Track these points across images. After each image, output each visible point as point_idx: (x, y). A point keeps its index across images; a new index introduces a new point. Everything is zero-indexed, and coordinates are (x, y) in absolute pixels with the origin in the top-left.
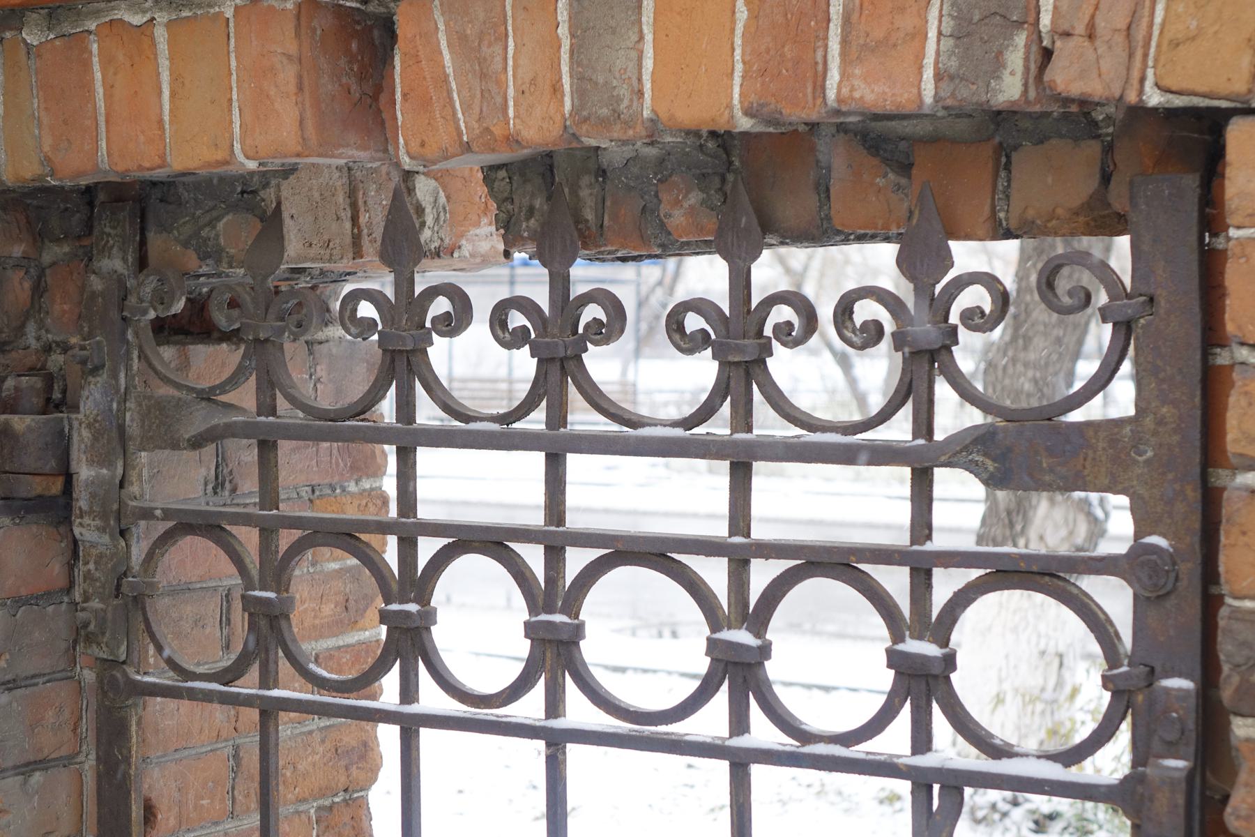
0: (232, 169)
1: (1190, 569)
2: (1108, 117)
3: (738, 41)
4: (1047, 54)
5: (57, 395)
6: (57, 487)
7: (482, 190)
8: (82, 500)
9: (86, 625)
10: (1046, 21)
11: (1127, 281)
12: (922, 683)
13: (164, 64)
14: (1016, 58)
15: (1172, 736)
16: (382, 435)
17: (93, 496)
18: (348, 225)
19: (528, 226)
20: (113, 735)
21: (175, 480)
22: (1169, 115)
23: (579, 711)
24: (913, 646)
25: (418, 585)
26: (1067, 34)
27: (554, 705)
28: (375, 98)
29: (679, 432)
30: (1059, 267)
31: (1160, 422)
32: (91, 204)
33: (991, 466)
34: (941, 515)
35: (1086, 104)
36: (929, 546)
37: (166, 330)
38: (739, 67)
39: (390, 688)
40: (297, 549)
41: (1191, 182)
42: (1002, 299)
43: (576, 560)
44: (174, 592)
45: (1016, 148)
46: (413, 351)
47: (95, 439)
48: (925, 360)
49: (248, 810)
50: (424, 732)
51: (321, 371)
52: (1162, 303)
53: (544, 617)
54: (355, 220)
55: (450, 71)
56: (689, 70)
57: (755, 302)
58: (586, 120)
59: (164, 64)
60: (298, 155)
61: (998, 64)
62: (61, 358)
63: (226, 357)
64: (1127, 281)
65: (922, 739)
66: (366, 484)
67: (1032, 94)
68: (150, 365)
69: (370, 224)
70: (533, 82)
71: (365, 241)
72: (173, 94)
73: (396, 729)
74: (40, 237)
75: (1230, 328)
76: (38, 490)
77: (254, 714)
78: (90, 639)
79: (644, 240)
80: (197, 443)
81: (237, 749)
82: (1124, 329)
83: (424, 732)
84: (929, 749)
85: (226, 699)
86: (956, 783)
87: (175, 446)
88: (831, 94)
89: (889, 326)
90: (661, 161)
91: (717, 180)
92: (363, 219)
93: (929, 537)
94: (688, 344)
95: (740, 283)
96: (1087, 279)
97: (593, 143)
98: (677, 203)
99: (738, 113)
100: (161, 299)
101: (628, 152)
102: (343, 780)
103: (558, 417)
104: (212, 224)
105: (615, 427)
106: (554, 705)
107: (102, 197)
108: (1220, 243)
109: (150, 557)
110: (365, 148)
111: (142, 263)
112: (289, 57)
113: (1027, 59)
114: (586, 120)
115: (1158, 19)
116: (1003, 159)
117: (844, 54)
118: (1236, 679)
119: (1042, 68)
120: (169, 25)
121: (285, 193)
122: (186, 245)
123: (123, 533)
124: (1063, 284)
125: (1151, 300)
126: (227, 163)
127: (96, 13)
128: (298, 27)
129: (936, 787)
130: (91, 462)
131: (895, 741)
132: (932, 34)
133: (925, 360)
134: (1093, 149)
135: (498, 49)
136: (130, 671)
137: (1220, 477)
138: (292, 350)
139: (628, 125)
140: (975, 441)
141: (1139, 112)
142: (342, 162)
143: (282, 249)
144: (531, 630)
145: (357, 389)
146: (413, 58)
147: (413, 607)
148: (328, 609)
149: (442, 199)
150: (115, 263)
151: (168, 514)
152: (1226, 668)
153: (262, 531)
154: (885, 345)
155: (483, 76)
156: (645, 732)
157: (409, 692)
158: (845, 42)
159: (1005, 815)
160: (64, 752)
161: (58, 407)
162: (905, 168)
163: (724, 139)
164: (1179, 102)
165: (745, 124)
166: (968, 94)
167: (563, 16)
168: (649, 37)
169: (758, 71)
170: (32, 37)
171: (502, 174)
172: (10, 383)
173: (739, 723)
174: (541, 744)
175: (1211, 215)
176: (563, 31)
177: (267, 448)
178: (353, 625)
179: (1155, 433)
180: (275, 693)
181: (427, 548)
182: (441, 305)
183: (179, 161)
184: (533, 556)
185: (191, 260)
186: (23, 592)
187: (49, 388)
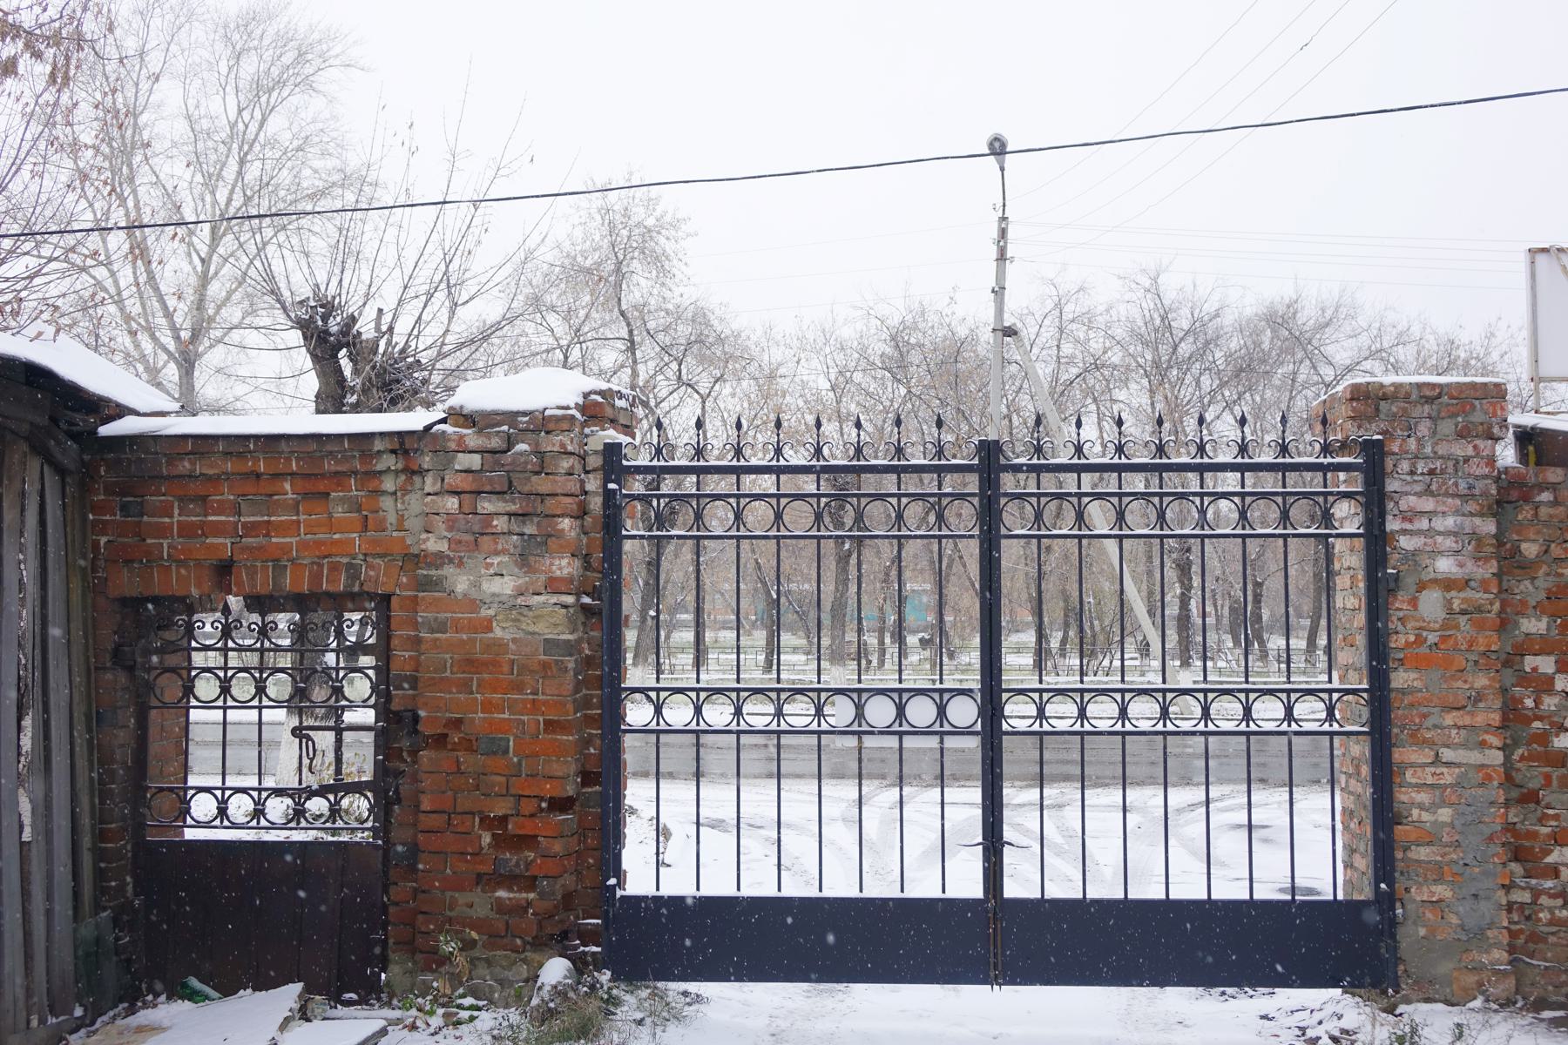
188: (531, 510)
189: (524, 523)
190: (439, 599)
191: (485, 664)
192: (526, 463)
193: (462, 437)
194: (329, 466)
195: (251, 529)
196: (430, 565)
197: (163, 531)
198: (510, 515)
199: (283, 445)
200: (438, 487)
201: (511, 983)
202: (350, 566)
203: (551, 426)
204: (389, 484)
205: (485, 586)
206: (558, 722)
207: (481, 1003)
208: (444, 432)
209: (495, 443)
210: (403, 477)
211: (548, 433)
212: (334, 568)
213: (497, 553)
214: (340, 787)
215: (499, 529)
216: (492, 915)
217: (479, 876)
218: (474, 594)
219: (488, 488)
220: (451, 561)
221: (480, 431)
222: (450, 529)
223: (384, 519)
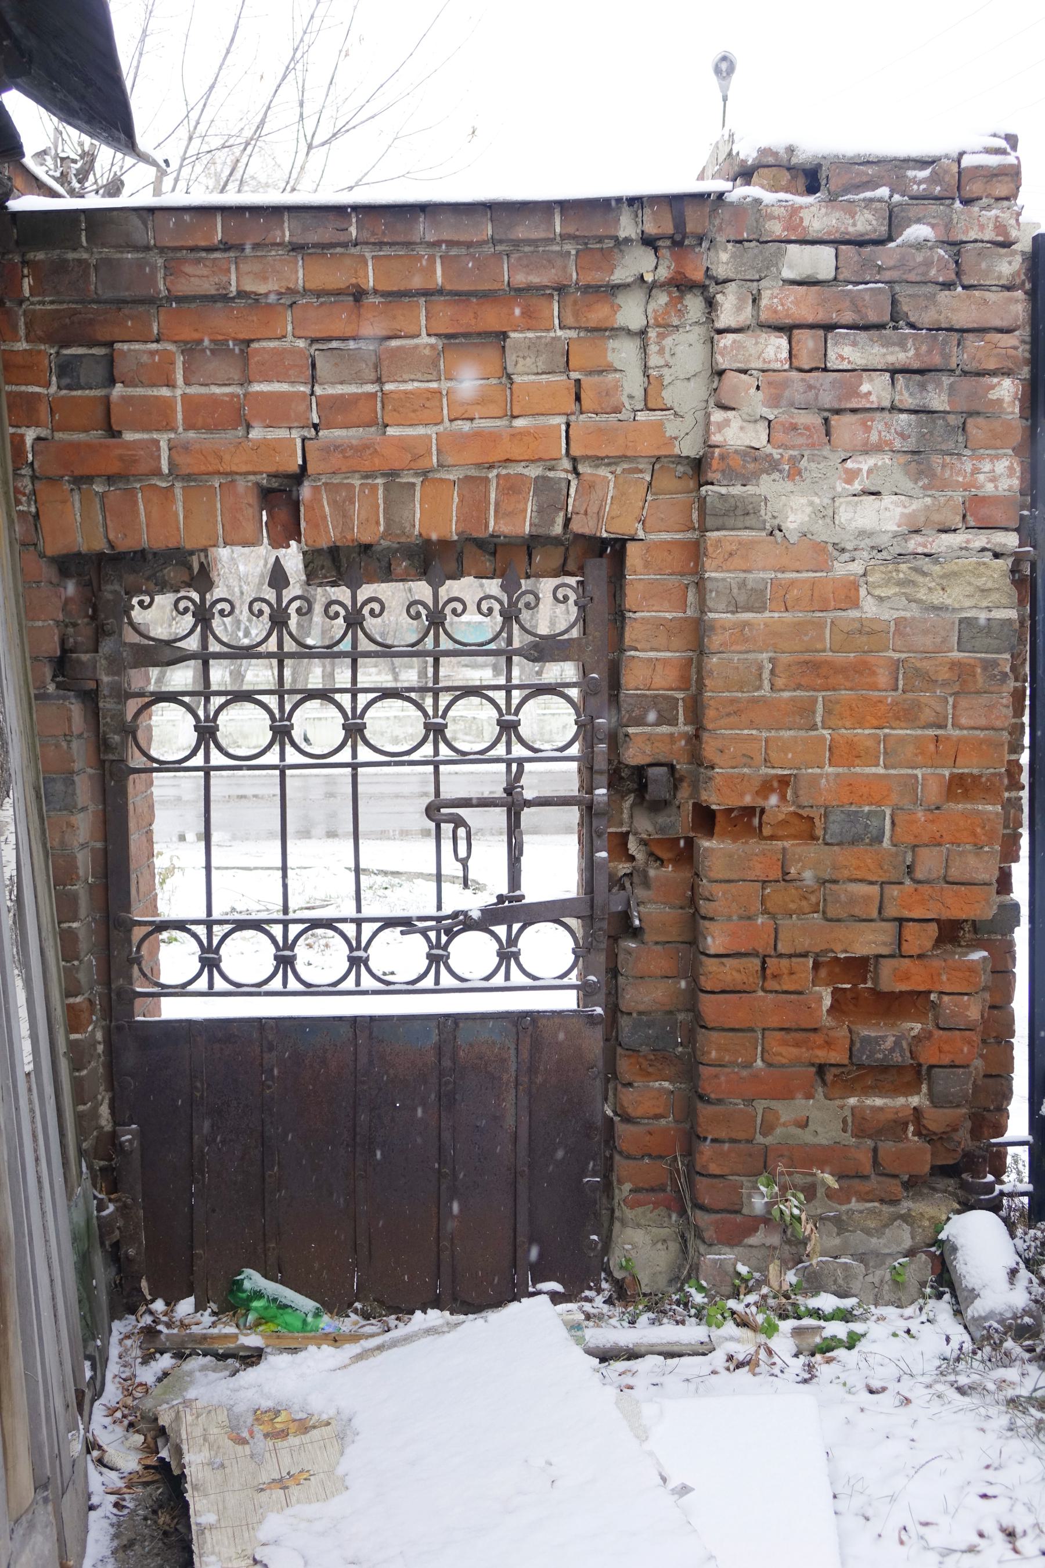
10: (570, 508)
14: (560, 520)
34: (348, 673)
52: (595, 600)
61: (553, 522)
72: (185, 517)
86: (521, 762)
106: (207, 758)
120: (183, 488)
130: (107, 675)
154: (190, 613)
155: (344, 516)
158: (496, 511)
166: (541, 531)
176: (381, 501)
188: (937, 360)
189: (923, 387)
190: (747, 546)
191: (843, 670)
192: (928, 264)
193: (795, 210)
194: (513, 273)
195: (336, 410)
196: (733, 475)
197: (158, 416)
198: (894, 372)
199: (423, 229)
200: (746, 315)
201: (880, 1258)
202: (542, 482)
203: (973, 189)
204: (631, 312)
205: (844, 515)
206: (976, 778)
207: (849, 1303)
208: (758, 201)
209: (865, 223)
210: (662, 299)
211: (966, 202)
212: (511, 487)
213: (867, 450)
214: (511, 913)
215: (874, 401)
216: (849, 1140)
217: (821, 1069)
218: (823, 533)
219: (848, 317)
220: (773, 466)
221: (832, 199)
222: (774, 402)
223: (618, 386)
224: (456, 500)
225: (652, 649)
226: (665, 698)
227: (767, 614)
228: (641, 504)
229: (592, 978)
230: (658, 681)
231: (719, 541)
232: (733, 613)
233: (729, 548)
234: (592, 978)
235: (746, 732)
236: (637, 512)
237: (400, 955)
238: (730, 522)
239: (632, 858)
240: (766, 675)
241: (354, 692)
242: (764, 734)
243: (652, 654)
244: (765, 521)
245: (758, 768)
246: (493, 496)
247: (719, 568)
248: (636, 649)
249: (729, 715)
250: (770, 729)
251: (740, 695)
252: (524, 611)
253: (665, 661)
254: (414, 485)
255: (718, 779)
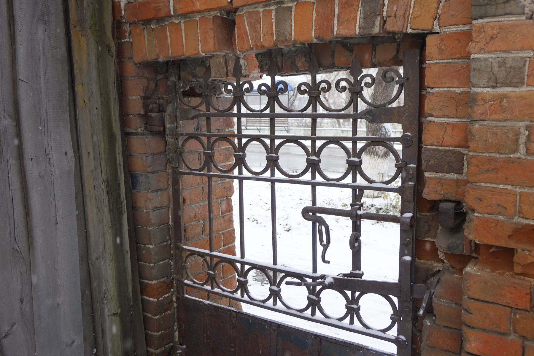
0: (199, 56)
1: (416, 140)
2: (399, 37)
3: (314, 21)
4: (385, 22)
5: (161, 109)
6: (162, 129)
7: (255, 59)
8: (167, 132)
9: (169, 159)
10: (385, 13)
11: (402, 75)
12: (354, 168)
13: (183, 31)
14: (378, 23)
15: (411, 177)
16: (234, 115)
17: (170, 131)
18: (225, 69)
19: (266, 68)
20: (176, 183)
21: (189, 127)
22: (413, 35)
23: (278, 175)
24: (352, 159)
25: (242, 148)
26: (390, 17)
27: (273, 174)
28: (231, 39)
29: (300, 113)
30: (387, 72)
31: (409, 107)
32: (168, 65)
33: (370, 118)
35: (393, 33)
36: (356, 137)
37: (186, 94)
38: (314, 27)
39: (236, 172)
40: (215, 141)
41: (418, 51)
42: (373, 80)
43: (277, 142)
44: (188, 152)
45: (377, 45)
46: (240, 96)
47: (170, 118)
48: (356, 92)
49: (205, 200)
50: (244, 181)
51: (220, 104)
53: (270, 155)
54: (227, 68)
55: (248, 31)
56: (301, 27)
57: (317, 82)
58: (279, 41)
59: (183, 31)
60: (214, 52)
61: (374, 24)
62: (162, 101)
63: (198, 100)
64: (402, 75)
65: (354, 180)
66: (230, 129)
67: (381, 31)
68: (182, 102)
69: (230, 70)
70: (267, 33)
71: (229, 73)
72: (185, 39)
73: (238, 180)
74: (156, 73)
75: (426, 84)
76: (158, 129)
77: (206, 179)
78: (170, 162)
79: (292, 70)
80: (192, 118)
81: (203, 187)
82: (401, 86)
83: (244, 181)
84: (356, 182)
85: (200, 175)
86: (362, 189)
87: (188, 119)
88: (335, 33)
89: (348, 87)
90: (296, 51)
91: (308, 55)
92: (229, 68)
93: (356, 135)
94: (303, 93)
95: (314, 79)
96: (393, 74)
97: (280, 47)
98: (299, 61)
99: (314, 38)
100: (184, 87)
101: (288, 49)
102: (226, 194)
103: (273, 110)
104: (195, 69)
105: (286, 112)
106: (273, 174)
107: (170, 64)
108: (424, 66)
109: (183, 144)
110: (229, 50)
111: (179, 78)
112: (212, 29)
113: (380, 23)
114: (279, 41)
115: (411, 12)
116: (374, 48)
117: (338, 24)
118: (425, 164)
119: (384, 25)
120: (184, 22)
121: (211, 62)
122: (189, 74)
123: (177, 139)
124: (388, 75)
125: (408, 79)
126: (198, 54)
127: (168, 20)
128: (213, 22)
129: (357, 190)
130: (169, 123)
131: (348, 180)
132: (358, 18)
133: (356, 92)
134: (395, 45)
135: (259, 25)
136: (179, 169)
137: (423, 120)
138: (214, 99)
139: (288, 42)
140: (367, 112)
141: (406, 35)
142: (224, 54)
143: (210, 74)
144: (267, 158)
145: (228, 105)
146: (239, 29)
147: (241, 153)
148: (222, 157)
149: (246, 64)
150: (173, 79)
151: (187, 134)
152: (423, 161)
153: (208, 137)
154: (347, 90)
155: (256, 32)
156: (293, 179)
157: (240, 172)
158: (338, 21)
159: (370, 209)
160: (165, 187)
161: (162, 112)
162: (352, 51)
163: (311, 45)
164: (415, 32)
165: (315, 41)
167: (273, 17)
168: (293, 21)
169: (318, 28)
170: (153, 27)
171: (260, 56)
172: (151, 106)
173: (314, 177)
174: (270, 183)
175: (422, 61)
176: (274, 20)
177: (208, 119)
178: (228, 160)
179: (408, 109)
180: (211, 173)
181: (244, 140)
182: (247, 86)
183: (187, 54)
184: (268, 141)
185: (190, 78)
186: (155, 152)
187: (159, 107)
214: (352, 285)
224: (315, 15)
225: (444, 116)
226: (454, 152)
227: (525, 88)
228: (436, 5)
229: (402, 337)
230: (448, 140)
231: (482, 27)
232: (493, 87)
233: (490, 33)
234: (402, 337)
235: (502, 186)
236: (433, 11)
237: (295, 296)
238: (491, 10)
239: (442, 262)
240: (522, 139)
241: (273, 139)
242: (518, 190)
243: (444, 120)
244: (524, 7)
245: (512, 217)
246: (336, 10)
247: (481, 50)
248: (432, 116)
249: (487, 171)
250: (523, 186)
251: (498, 155)
252: (365, 88)
253: (453, 125)
254: (291, 8)
255: (476, 221)
